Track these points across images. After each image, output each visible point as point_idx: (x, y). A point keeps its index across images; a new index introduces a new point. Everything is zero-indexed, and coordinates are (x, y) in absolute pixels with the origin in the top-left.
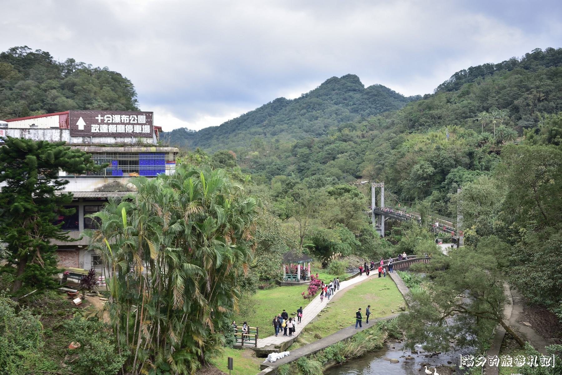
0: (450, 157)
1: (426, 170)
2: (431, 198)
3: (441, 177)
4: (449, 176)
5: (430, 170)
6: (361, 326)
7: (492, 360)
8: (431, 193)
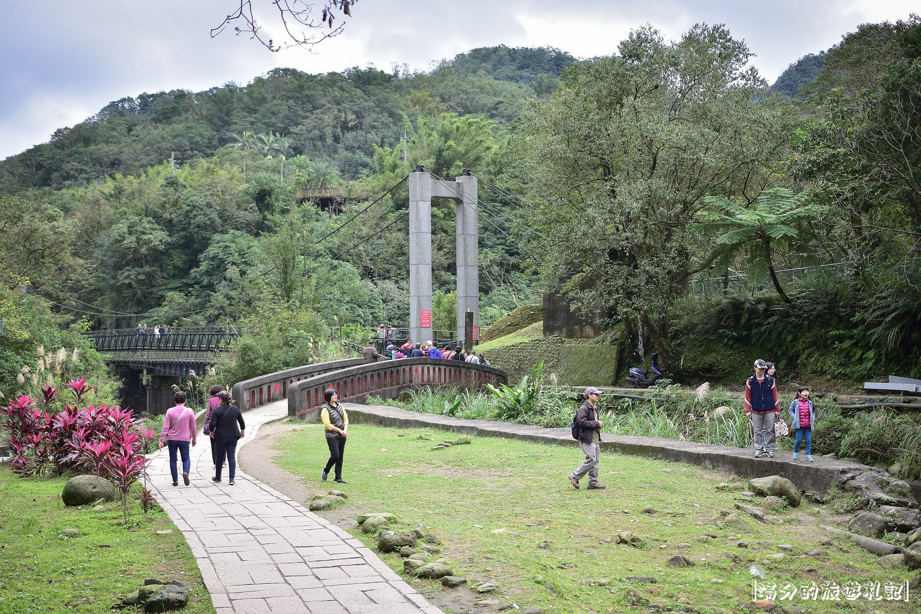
0: (209, 205)
1: (145, 237)
2: (162, 312)
3: (184, 257)
4: (212, 250)
5: (158, 237)
6: (338, 478)
7: (807, 589)
8: (162, 298)
